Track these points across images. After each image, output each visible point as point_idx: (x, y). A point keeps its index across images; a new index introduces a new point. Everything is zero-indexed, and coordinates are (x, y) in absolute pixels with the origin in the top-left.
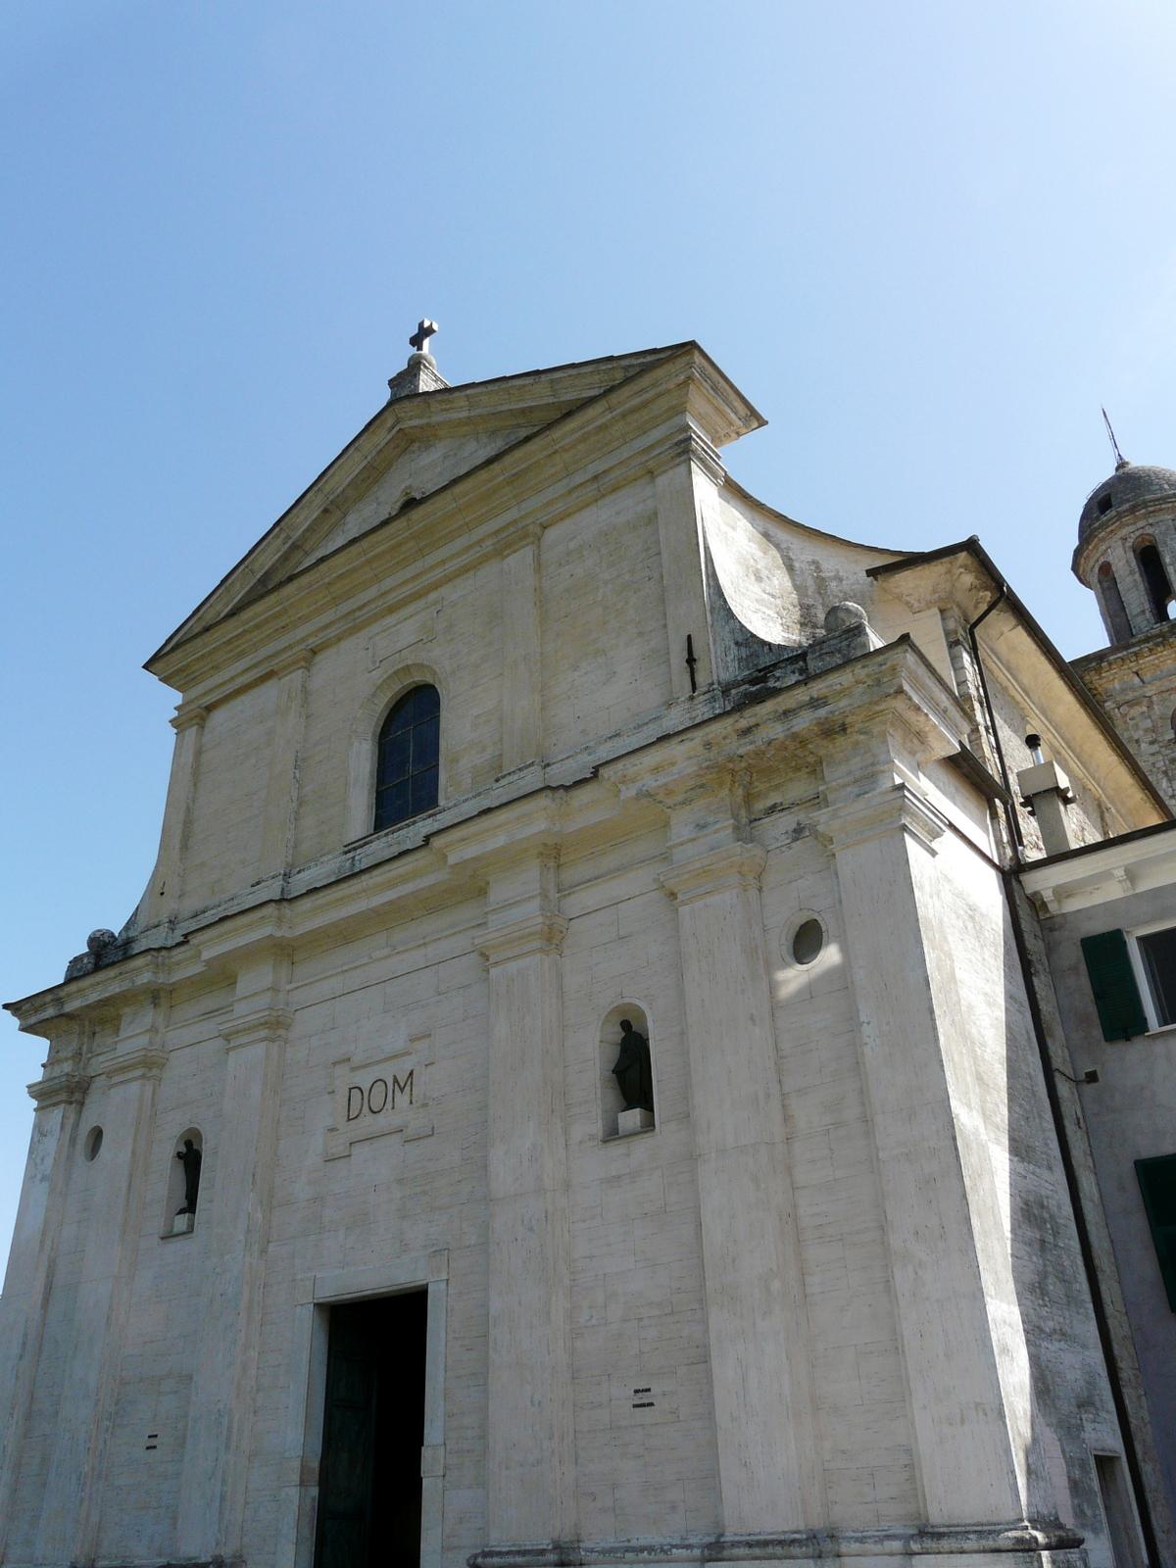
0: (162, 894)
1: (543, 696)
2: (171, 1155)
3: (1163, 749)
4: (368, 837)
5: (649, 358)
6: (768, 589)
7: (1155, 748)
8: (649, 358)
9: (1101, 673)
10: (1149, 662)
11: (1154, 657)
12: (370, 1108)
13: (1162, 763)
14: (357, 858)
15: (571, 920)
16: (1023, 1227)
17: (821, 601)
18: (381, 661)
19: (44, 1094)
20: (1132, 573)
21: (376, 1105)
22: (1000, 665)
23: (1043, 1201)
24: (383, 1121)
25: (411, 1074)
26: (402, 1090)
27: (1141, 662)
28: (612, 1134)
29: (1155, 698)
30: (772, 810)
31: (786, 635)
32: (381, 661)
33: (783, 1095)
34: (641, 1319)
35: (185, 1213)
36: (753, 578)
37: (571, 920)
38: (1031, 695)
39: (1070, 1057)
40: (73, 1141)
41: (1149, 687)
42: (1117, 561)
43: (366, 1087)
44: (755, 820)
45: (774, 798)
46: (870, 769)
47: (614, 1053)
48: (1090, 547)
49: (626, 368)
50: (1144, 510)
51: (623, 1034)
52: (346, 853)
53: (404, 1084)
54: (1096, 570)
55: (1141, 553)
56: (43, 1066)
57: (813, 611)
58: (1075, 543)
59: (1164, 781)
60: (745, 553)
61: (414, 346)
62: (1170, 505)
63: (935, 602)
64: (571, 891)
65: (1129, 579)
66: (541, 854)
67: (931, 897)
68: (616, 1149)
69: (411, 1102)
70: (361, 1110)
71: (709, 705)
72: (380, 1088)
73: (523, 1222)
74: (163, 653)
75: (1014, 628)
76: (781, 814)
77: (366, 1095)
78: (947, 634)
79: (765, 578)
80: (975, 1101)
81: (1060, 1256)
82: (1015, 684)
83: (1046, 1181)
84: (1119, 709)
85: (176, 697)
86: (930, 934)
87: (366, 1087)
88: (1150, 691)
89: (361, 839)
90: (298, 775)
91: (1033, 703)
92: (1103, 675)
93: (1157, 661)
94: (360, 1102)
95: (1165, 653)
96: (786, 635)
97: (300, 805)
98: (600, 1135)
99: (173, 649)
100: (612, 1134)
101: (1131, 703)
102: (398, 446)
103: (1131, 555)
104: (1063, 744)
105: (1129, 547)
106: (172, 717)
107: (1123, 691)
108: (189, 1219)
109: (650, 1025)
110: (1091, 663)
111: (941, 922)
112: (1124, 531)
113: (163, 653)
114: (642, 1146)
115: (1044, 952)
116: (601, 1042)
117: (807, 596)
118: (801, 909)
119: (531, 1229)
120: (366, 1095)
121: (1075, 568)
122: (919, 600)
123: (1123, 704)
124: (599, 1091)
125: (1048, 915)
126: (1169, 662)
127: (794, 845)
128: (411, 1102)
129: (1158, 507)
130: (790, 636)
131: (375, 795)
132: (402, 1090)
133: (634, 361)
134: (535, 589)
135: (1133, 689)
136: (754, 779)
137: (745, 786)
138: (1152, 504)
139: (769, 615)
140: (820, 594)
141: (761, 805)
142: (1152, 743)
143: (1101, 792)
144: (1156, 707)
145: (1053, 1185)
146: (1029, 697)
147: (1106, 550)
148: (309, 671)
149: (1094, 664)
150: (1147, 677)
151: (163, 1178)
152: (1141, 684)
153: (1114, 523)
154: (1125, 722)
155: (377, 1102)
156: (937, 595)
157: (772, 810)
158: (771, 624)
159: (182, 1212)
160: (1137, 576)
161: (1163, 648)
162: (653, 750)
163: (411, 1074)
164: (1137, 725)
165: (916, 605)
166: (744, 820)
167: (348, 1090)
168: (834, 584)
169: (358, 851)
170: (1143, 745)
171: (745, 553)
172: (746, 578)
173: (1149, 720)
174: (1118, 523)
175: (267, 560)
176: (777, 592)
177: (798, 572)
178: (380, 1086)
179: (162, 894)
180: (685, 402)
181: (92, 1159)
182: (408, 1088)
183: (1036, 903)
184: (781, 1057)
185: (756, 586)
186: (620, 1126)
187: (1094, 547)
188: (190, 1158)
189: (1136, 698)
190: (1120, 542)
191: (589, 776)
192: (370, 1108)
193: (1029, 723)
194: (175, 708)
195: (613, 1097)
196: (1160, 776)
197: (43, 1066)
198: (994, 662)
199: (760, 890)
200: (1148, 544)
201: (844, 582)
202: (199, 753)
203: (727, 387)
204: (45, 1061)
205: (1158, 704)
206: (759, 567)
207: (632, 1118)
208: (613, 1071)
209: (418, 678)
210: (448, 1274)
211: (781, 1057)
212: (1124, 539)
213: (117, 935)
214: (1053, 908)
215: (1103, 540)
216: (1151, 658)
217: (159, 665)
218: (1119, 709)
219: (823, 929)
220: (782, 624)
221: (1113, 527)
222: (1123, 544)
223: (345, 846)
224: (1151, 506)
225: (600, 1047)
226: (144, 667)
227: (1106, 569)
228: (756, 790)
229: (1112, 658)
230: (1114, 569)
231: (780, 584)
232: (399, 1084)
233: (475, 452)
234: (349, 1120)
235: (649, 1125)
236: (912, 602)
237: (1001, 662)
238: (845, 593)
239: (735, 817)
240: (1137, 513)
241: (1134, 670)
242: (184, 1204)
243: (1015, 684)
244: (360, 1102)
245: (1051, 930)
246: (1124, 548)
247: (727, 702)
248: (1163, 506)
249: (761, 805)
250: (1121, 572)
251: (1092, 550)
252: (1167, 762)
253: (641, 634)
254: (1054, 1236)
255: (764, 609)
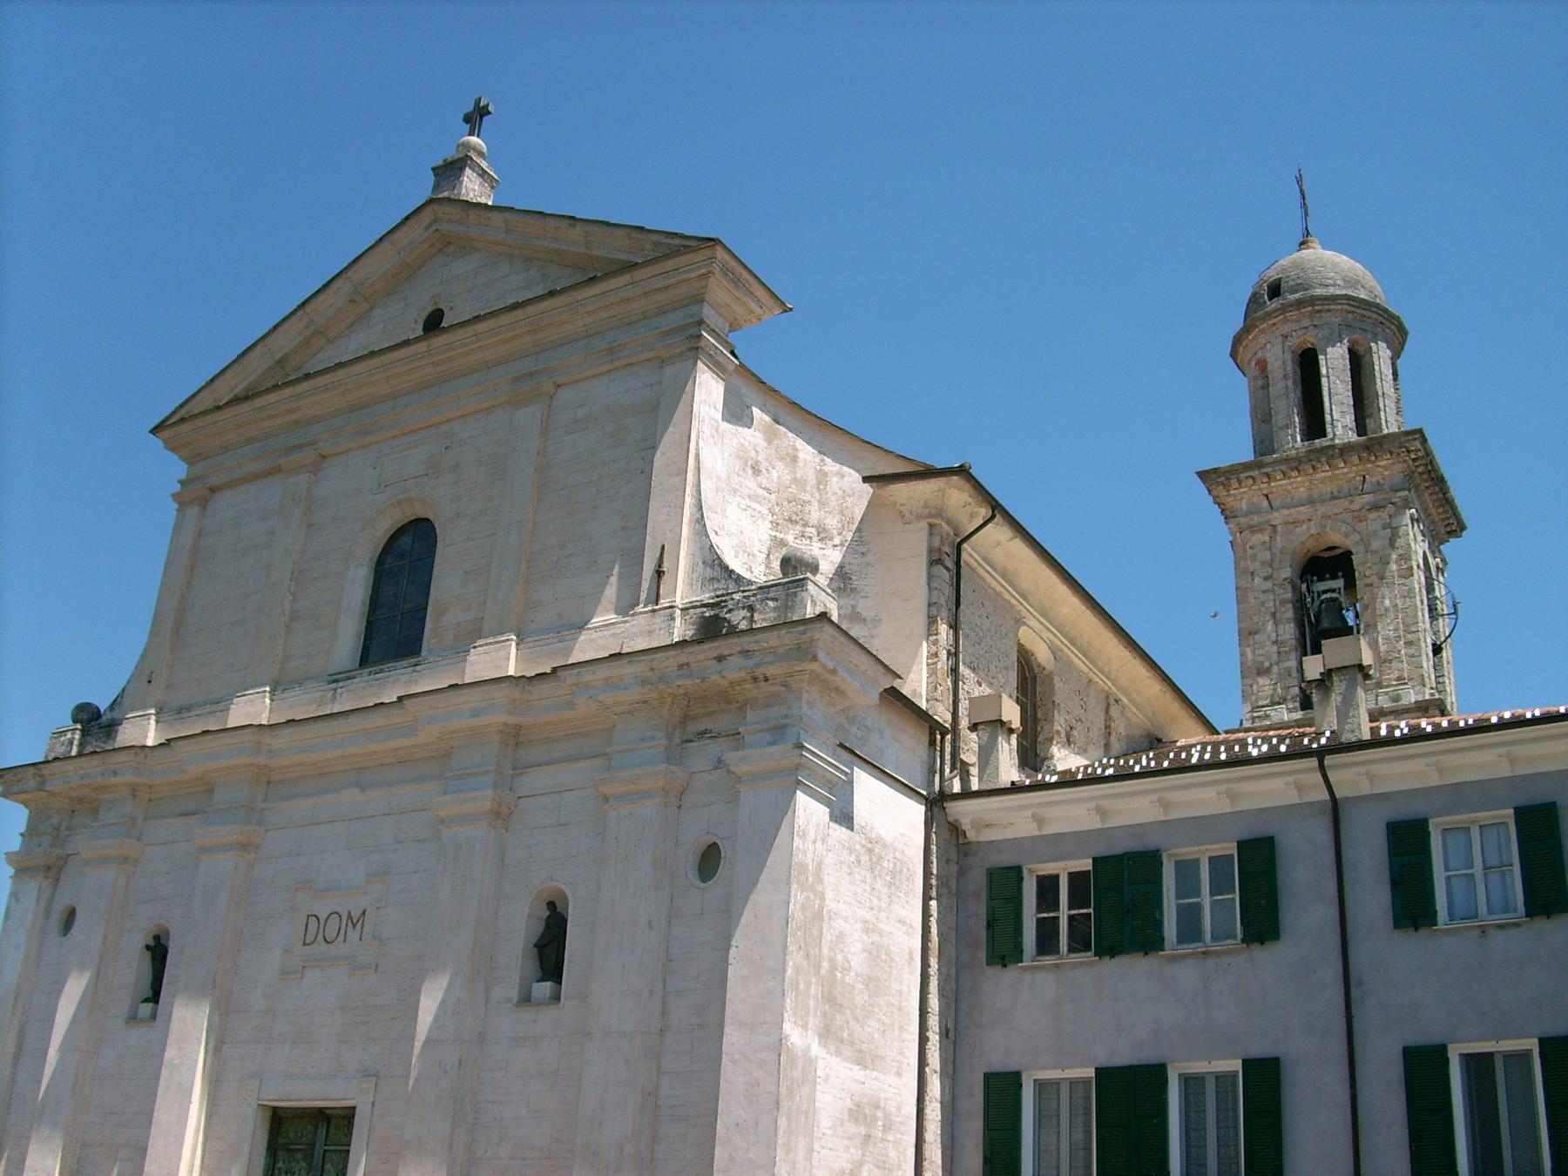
0: (149, 682)
1: (529, 568)
2: (140, 946)
3: (1276, 588)
4: (351, 671)
5: (677, 241)
6: (765, 483)
7: (1269, 584)
8: (677, 241)
9: (1228, 491)
10: (1281, 486)
11: (1288, 481)
12: (324, 938)
13: (1272, 604)
14: (339, 690)
15: (520, 798)
16: (847, 1124)
17: (818, 497)
18: (386, 486)
19: (23, 866)
20: (1285, 377)
21: (330, 934)
22: (993, 573)
23: (880, 1102)
24: (333, 950)
25: (364, 912)
26: (354, 926)
27: (1272, 484)
28: (526, 999)
29: (1279, 529)
30: (702, 734)
31: (774, 533)
32: (386, 486)
33: (665, 992)
34: (524, 1159)
35: (149, 1002)
36: (750, 471)
37: (520, 798)
38: (1030, 599)
39: (956, 974)
40: (48, 914)
41: (1276, 514)
42: (1273, 360)
43: (323, 917)
44: (687, 741)
45: (706, 724)
46: (782, 722)
47: (539, 928)
48: (1250, 337)
49: (656, 244)
50: (1310, 308)
51: (548, 913)
52: (329, 683)
53: (355, 921)
54: (1253, 364)
55: (1301, 356)
56: (22, 834)
57: (807, 508)
58: (1239, 324)
59: (1271, 623)
60: (747, 444)
61: (467, 123)
62: (1340, 307)
63: (925, 517)
64: (524, 770)
65: (1281, 384)
66: (502, 732)
67: (814, 842)
68: (527, 1014)
69: (361, 939)
70: (316, 938)
71: (666, 623)
72: (334, 920)
73: (440, 1065)
74: (168, 423)
75: (1011, 540)
76: (708, 741)
77: (322, 922)
78: (930, 551)
79: (764, 471)
80: (814, 1021)
81: (885, 1149)
82: (1011, 590)
83: (890, 1086)
84: (1241, 533)
85: (180, 469)
86: (802, 879)
87: (323, 917)
88: (1277, 518)
89: (344, 672)
90: (292, 588)
91: (1032, 607)
92: (1232, 492)
93: (1289, 487)
94: (316, 930)
95: (1299, 479)
96: (774, 533)
97: (292, 619)
98: (515, 999)
99: (182, 420)
100: (526, 999)
101: (1258, 529)
102: (433, 245)
103: (1288, 356)
104: (1066, 642)
105: (1290, 347)
106: (174, 492)
107: (1249, 513)
108: (152, 1009)
109: (570, 910)
110: (1220, 477)
111: (820, 865)
112: (1286, 329)
113: (168, 423)
114: (548, 1015)
115: (955, 874)
116: (529, 916)
117: (805, 491)
118: (708, 833)
119: (446, 1072)
120: (322, 922)
121: (1234, 354)
122: (911, 512)
123: (1246, 529)
124: (520, 960)
125: (966, 841)
126: (1302, 489)
127: (713, 772)
128: (361, 939)
129: (1326, 307)
130: (778, 534)
131: (365, 624)
132: (354, 926)
133: (663, 239)
134: (539, 453)
135: (1259, 512)
136: (691, 703)
137: (682, 709)
138: (1319, 303)
139: (759, 512)
140: (819, 489)
141: (693, 728)
142: (1266, 579)
143: (1110, 684)
144: (1279, 539)
145: (898, 1089)
146: (1027, 601)
147: (1265, 345)
148: (316, 476)
149: (1223, 478)
150: (1276, 503)
151: (134, 969)
152: (1270, 509)
153: (1279, 315)
154: (1245, 550)
155: (331, 932)
156: (928, 510)
157: (702, 734)
158: (759, 521)
159: (146, 1000)
160: (1290, 383)
161: (1297, 474)
162: (605, 665)
163: (364, 912)
164: (1255, 555)
165: (907, 515)
166: (677, 740)
167: (305, 917)
168: (835, 479)
169: (341, 684)
170: (1257, 580)
171: (747, 444)
172: (741, 473)
173: (1269, 552)
174: (1282, 317)
175: (284, 342)
176: (774, 488)
177: (801, 465)
178: (334, 920)
179: (149, 682)
180: (705, 293)
181: (65, 935)
182: (359, 926)
183: (955, 829)
184: (670, 961)
185: (752, 480)
186: (532, 995)
187: (1253, 338)
188: (158, 952)
189: (1259, 524)
190: (1280, 339)
191: (549, 671)
192: (324, 938)
193: (1024, 624)
194: (179, 482)
195: (533, 967)
196: (1268, 617)
197: (22, 834)
198: (988, 572)
199: (680, 807)
200: (1310, 346)
201: (845, 479)
202: (199, 535)
203: (750, 279)
204: (23, 831)
205: (1281, 536)
206: (759, 459)
207: (544, 988)
208: (535, 945)
209: (420, 512)
210: (374, 1097)
211: (670, 961)
212: (1285, 337)
213: (102, 710)
214: (971, 835)
215: (1263, 332)
216: (1285, 482)
217: (167, 434)
218: (1241, 533)
219: (723, 855)
220: (772, 522)
221: (1276, 320)
222: (1283, 342)
223: (330, 675)
224: (1318, 305)
225: (527, 921)
226: (150, 432)
227: (1262, 365)
228: (692, 713)
229: (1242, 475)
230: (1269, 368)
231: (779, 478)
232: (352, 921)
233: (508, 276)
234: (304, 944)
235: (556, 998)
236: (905, 512)
237: (995, 570)
238: (844, 491)
239: (669, 738)
240: (1303, 311)
241: (1264, 492)
242: (149, 993)
243: (1011, 590)
244: (316, 930)
245: (966, 855)
246: (1283, 347)
247: (683, 621)
248: (1332, 307)
249: (693, 728)
250: (1275, 374)
251: (1251, 341)
252: (1278, 603)
253: (624, 528)
254: (884, 1130)
255: (755, 505)
